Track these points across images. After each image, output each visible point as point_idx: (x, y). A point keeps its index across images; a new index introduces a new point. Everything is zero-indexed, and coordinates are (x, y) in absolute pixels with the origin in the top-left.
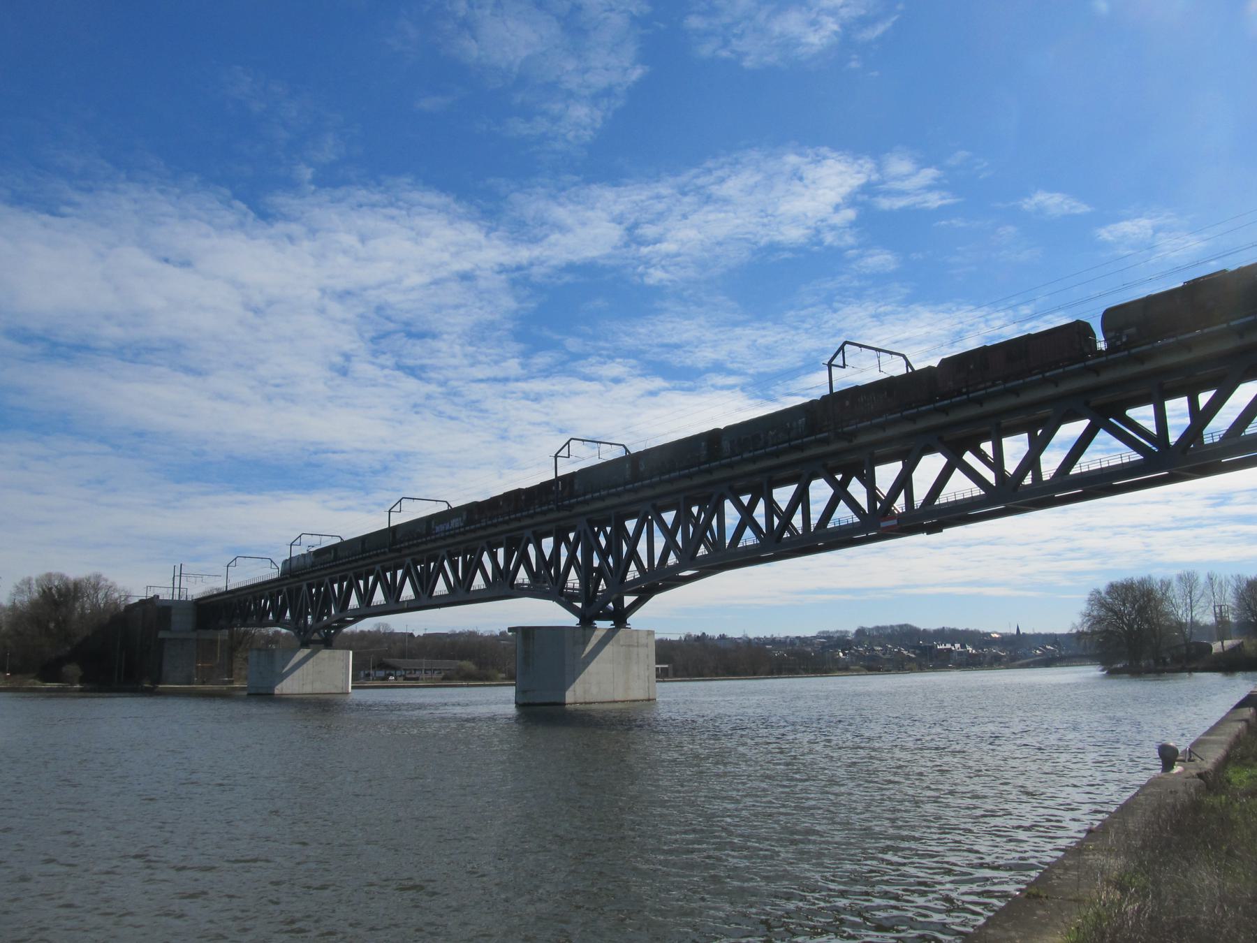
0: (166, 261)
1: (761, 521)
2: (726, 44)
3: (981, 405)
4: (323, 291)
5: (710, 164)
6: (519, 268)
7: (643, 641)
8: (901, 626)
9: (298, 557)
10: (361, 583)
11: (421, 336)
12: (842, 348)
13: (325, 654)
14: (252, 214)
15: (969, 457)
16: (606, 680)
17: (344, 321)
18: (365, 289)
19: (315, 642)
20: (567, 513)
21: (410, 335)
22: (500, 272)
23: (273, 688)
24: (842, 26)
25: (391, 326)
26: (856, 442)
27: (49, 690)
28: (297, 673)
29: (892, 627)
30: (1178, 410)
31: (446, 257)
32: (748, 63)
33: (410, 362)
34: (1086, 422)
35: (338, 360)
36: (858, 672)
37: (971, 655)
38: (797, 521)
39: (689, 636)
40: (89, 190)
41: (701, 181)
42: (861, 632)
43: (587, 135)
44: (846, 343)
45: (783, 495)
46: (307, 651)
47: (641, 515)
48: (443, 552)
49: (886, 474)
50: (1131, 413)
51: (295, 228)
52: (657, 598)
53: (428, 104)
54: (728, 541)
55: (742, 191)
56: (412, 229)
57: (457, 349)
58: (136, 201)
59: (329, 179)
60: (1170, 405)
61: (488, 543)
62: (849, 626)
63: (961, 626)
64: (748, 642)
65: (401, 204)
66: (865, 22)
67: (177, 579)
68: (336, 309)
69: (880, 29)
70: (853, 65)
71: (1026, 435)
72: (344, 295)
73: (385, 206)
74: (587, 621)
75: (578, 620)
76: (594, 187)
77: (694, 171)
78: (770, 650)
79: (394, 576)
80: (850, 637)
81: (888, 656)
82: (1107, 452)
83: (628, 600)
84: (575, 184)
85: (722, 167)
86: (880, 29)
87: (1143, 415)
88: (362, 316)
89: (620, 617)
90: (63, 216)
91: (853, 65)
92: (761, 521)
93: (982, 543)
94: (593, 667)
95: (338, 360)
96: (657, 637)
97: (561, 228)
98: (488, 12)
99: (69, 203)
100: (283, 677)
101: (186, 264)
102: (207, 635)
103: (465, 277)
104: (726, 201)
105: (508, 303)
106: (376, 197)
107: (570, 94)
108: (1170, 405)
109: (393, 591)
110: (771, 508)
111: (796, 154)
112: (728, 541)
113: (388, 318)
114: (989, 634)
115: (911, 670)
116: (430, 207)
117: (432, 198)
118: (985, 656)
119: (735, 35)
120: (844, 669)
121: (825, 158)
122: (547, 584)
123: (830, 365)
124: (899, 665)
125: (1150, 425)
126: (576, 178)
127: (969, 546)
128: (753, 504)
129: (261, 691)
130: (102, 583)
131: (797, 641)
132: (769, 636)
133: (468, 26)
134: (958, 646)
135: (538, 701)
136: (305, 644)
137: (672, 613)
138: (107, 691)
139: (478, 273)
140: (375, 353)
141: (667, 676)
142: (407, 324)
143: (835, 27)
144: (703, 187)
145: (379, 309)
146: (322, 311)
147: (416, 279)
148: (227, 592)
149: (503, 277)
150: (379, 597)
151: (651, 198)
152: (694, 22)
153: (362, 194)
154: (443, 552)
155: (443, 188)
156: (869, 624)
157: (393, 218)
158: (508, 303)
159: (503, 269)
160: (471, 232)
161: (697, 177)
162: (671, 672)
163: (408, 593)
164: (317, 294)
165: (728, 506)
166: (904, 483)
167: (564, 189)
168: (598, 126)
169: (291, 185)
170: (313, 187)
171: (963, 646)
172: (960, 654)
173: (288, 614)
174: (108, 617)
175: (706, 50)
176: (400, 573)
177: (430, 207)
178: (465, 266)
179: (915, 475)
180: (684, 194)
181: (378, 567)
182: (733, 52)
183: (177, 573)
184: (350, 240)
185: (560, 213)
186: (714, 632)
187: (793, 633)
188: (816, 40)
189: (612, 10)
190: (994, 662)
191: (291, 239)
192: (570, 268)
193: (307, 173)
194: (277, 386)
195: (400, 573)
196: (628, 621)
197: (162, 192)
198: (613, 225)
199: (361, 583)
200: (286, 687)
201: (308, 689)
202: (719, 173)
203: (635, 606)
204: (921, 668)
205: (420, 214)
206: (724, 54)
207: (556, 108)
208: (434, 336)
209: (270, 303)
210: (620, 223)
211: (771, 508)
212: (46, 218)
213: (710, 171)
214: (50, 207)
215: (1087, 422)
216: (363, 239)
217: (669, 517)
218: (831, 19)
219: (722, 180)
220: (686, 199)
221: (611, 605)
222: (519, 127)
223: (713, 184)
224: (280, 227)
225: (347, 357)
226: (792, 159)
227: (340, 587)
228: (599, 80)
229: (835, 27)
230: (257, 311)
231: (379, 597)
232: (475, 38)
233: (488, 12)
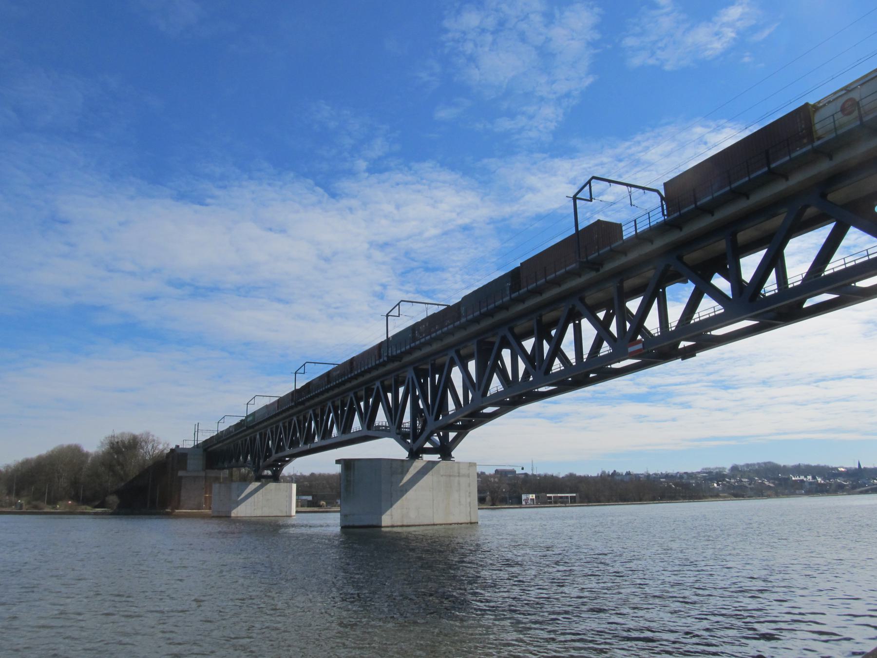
0: (271, 230)
2: (653, 54)
4: (372, 244)
5: (639, 138)
6: (504, 220)
7: (463, 471)
8: (765, 463)
9: (253, 414)
11: (434, 270)
12: (589, 182)
13: (272, 486)
14: (326, 195)
16: (429, 504)
17: (384, 263)
18: (398, 240)
19: (267, 477)
21: (427, 269)
22: (488, 224)
23: (230, 512)
24: (738, 33)
25: (415, 264)
26: (602, 271)
27: (96, 514)
28: (250, 500)
29: (758, 464)
31: (454, 215)
32: (668, 67)
33: (425, 288)
35: (378, 288)
36: (725, 498)
37: (820, 485)
39: (604, 472)
40: (224, 187)
41: (634, 149)
42: (735, 468)
43: (552, 126)
44: (594, 178)
46: (258, 484)
47: (456, 359)
51: (354, 203)
52: (473, 433)
53: (443, 114)
55: (661, 155)
56: (432, 198)
57: (458, 277)
58: (253, 192)
59: (377, 168)
62: (725, 464)
63: (814, 463)
64: (648, 476)
65: (424, 181)
66: (755, 29)
68: (378, 255)
69: (766, 32)
70: (746, 60)
72: (384, 246)
73: (414, 184)
74: (414, 454)
76: (556, 160)
77: (627, 144)
78: (661, 482)
80: (727, 472)
81: (752, 486)
83: (452, 435)
84: (544, 159)
85: (648, 139)
86: (766, 32)
88: (395, 259)
89: (445, 450)
90: (207, 205)
91: (746, 60)
93: (839, 400)
94: (411, 494)
95: (378, 288)
96: (479, 470)
97: (532, 189)
98: (486, 49)
99: (212, 197)
100: (238, 503)
101: (283, 231)
102: (213, 473)
103: (466, 228)
104: (650, 164)
105: (494, 244)
106: (409, 178)
107: (542, 99)
111: (703, 126)
113: (413, 260)
114: (836, 469)
115: (769, 496)
116: (444, 182)
117: (447, 176)
118: (831, 485)
119: (659, 48)
120: (715, 495)
121: (724, 127)
124: (760, 492)
126: (545, 155)
127: (828, 402)
129: (221, 514)
130: (151, 438)
131: (685, 476)
132: (664, 472)
133: (472, 59)
134: (810, 477)
135: (357, 524)
136: (258, 478)
138: (145, 514)
139: (475, 225)
140: (402, 283)
141: (575, 502)
142: (425, 263)
143: (733, 35)
144: (633, 155)
145: (407, 254)
146: (369, 257)
147: (433, 232)
149: (492, 226)
151: (597, 165)
152: (630, 42)
153: (399, 177)
155: (452, 168)
156: (741, 461)
157: (419, 191)
158: (494, 244)
159: (492, 221)
160: (471, 198)
161: (629, 148)
162: (578, 499)
164: (366, 246)
167: (535, 163)
168: (560, 119)
169: (351, 173)
170: (367, 174)
171: (814, 478)
172: (810, 483)
175: (636, 61)
177: (444, 182)
178: (465, 220)
180: (620, 161)
182: (657, 59)
184: (389, 208)
185: (532, 180)
186: (622, 470)
187: (682, 470)
188: (718, 46)
189: (573, 39)
190: (839, 489)
191: (351, 209)
192: (539, 217)
193: (362, 165)
194: (336, 308)
196: (453, 454)
197: (270, 185)
198: (570, 186)
200: (242, 511)
201: (258, 513)
202: (644, 144)
203: (457, 439)
204: (777, 495)
205: (436, 188)
206: (652, 62)
207: (531, 109)
208: (443, 269)
209: (335, 254)
210: (574, 184)
212: (197, 207)
213: (639, 143)
214: (200, 201)
216: (398, 207)
218: (730, 30)
219: (647, 149)
220: (621, 164)
222: (504, 124)
223: (640, 152)
224: (344, 202)
225: (384, 286)
226: (699, 130)
228: (562, 87)
229: (733, 35)
230: (327, 260)
232: (477, 67)
233: (486, 49)
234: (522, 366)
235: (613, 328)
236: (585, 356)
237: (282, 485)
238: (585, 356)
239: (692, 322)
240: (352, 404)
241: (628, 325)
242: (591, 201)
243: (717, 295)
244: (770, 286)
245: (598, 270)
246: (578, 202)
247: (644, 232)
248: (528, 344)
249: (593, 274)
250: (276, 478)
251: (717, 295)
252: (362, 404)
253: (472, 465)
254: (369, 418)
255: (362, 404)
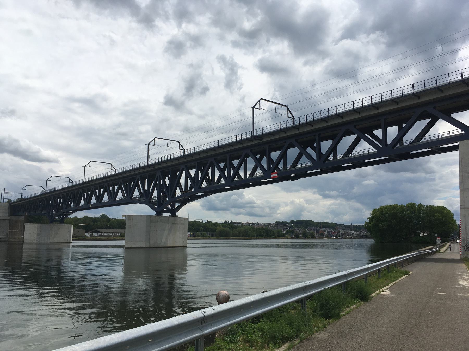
1: (265, 166)
3: (286, 133)
10: (97, 191)
12: (259, 101)
15: (309, 150)
20: (152, 168)
26: (262, 141)
30: (393, 131)
34: (355, 136)
38: (281, 166)
45: (275, 155)
47: (242, 157)
48: (183, 166)
49: (393, 131)
50: (375, 132)
54: (215, 181)
60: (389, 129)
61: (186, 166)
67: (3, 194)
71: (397, 126)
74: (159, 213)
75: (155, 213)
79: (114, 189)
82: (364, 147)
87: (378, 133)
89: (173, 212)
92: (265, 166)
108: (389, 129)
109: (113, 195)
110: (270, 161)
112: (215, 181)
122: (146, 198)
123: (253, 108)
125: (380, 137)
128: (261, 159)
137: (193, 211)
148: (84, 183)
150: (106, 198)
154: (138, 177)
163: (120, 196)
165: (250, 160)
166: (333, 150)
173: (72, 204)
174: (467, 42)
176: (116, 187)
179: (338, 146)
181: (92, 187)
183: (3, 192)
195: (116, 187)
199: (97, 191)
211: (270, 161)
215: (356, 136)
217: (222, 165)
221: (169, 206)
227: (100, 192)
231: (106, 198)
234: (189, 183)
235: (226, 173)
236: (248, 176)
237: (66, 226)
238: (248, 176)
239: (463, 132)
240: (92, 190)
241: (271, 166)
242: (260, 109)
243: (310, 157)
244: (331, 158)
245: (260, 140)
246: (255, 109)
247: (297, 126)
248: (192, 172)
249: (259, 141)
250: (62, 221)
251: (310, 157)
252: (85, 194)
253: (186, 219)
254: (88, 200)
255: (85, 194)
